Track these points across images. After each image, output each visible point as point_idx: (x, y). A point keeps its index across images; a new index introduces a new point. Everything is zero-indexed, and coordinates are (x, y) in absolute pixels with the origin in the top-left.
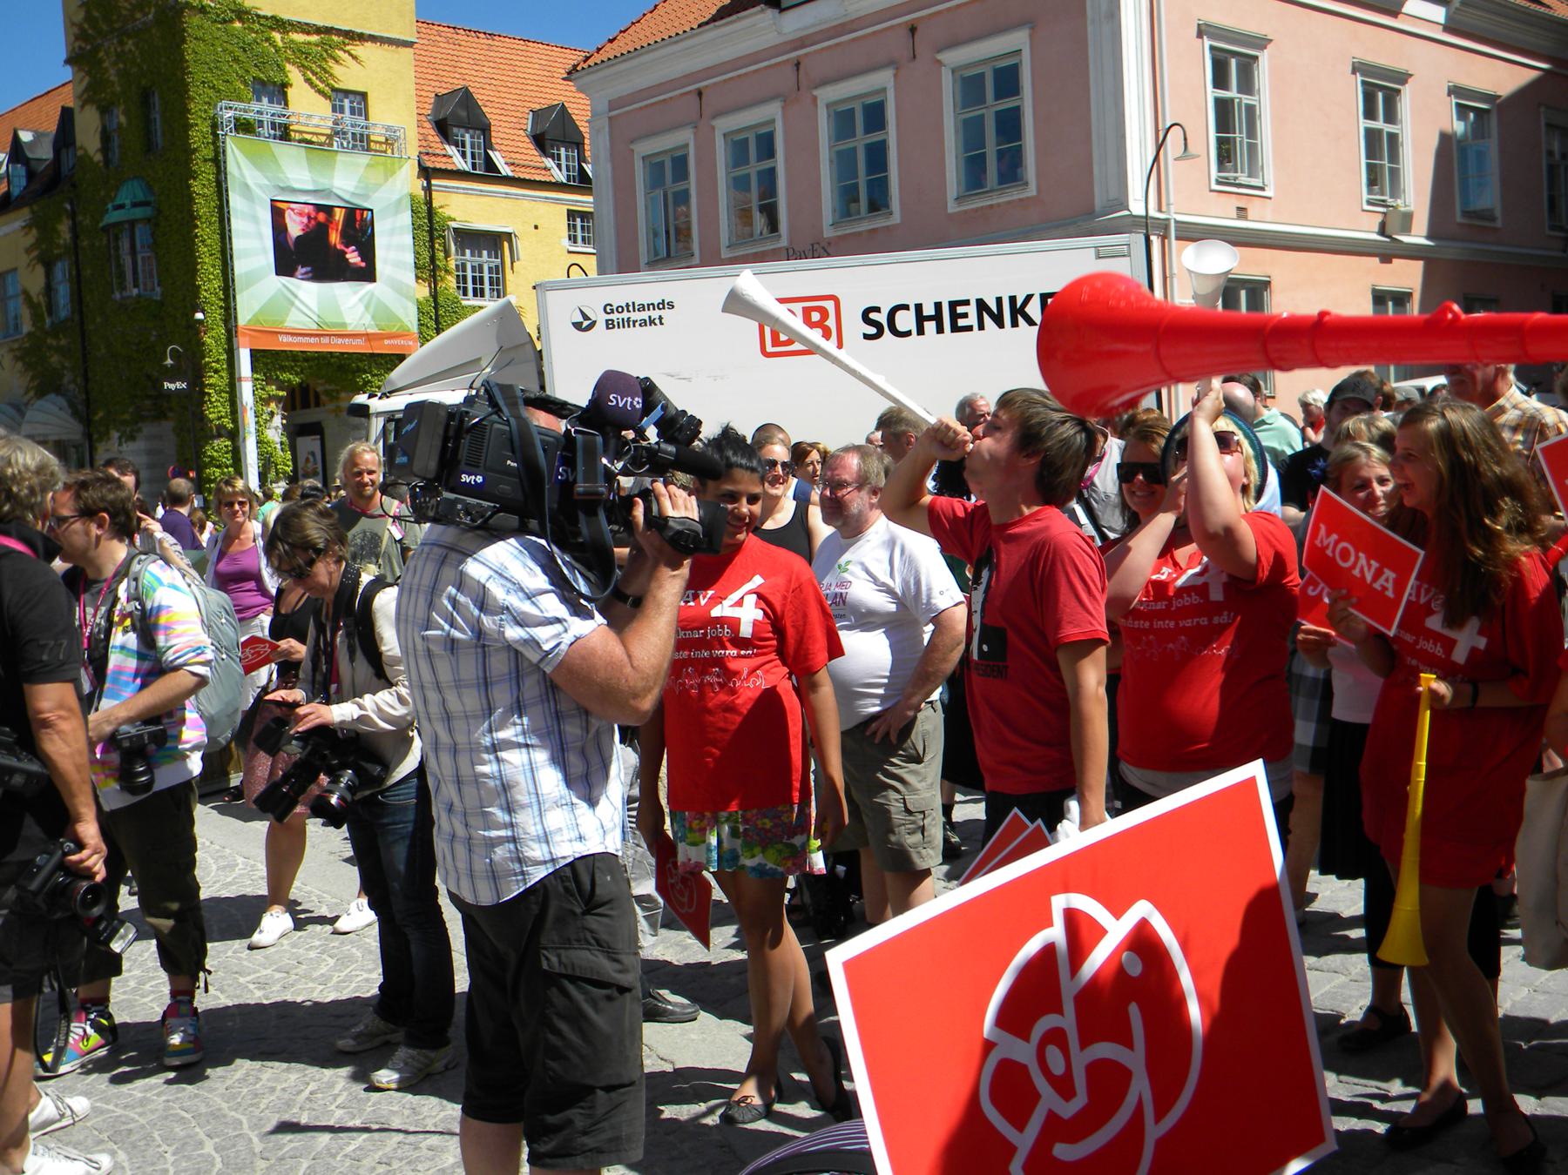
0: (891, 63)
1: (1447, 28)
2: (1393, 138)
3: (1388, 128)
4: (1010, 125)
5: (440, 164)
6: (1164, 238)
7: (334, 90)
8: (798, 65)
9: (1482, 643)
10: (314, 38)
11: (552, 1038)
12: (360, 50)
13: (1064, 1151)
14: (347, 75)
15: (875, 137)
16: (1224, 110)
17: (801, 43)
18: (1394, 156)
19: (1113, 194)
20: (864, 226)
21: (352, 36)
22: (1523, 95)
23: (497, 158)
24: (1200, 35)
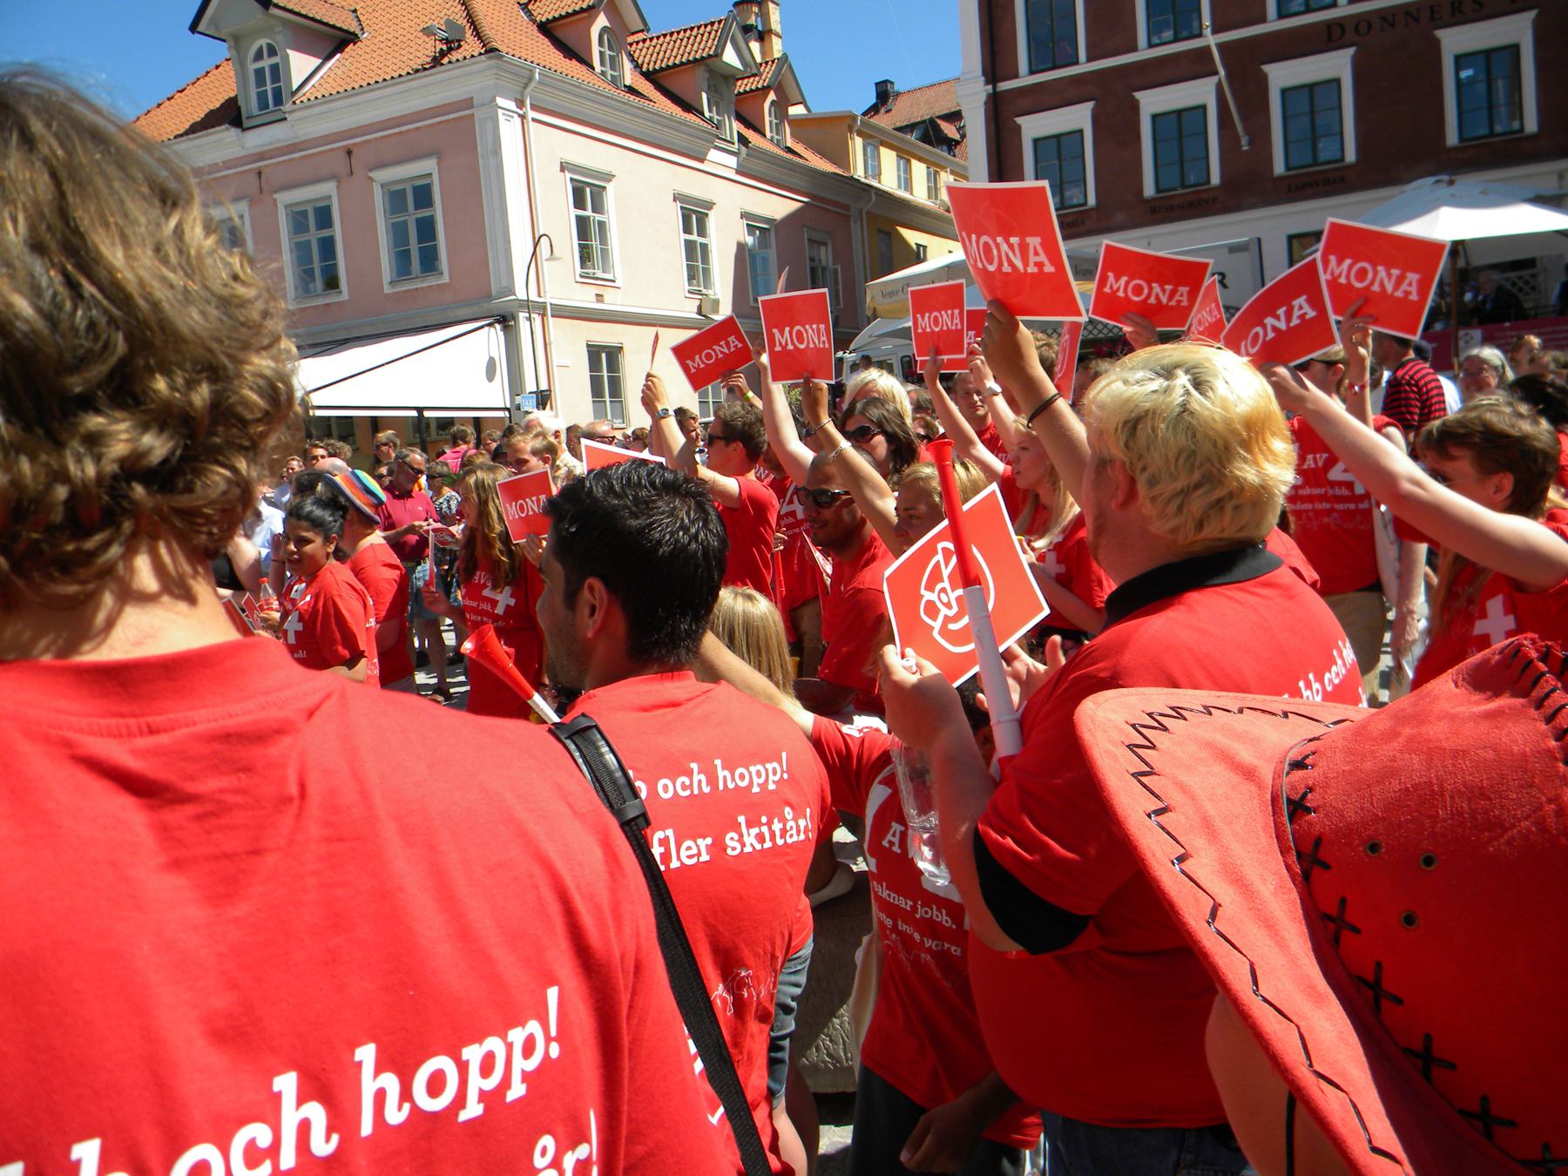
0: (333, 177)
1: (738, 172)
2: (704, 247)
3: (700, 240)
4: (427, 229)
6: (543, 316)
8: (260, 173)
9: (512, 602)
13: (952, 627)
15: (325, 233)
16: (582, 224)
17: (261, 156)
18: (706, 259)
19: (504, 283)
20: (321, 301)
22: (792, 218)
24: (562, 169)
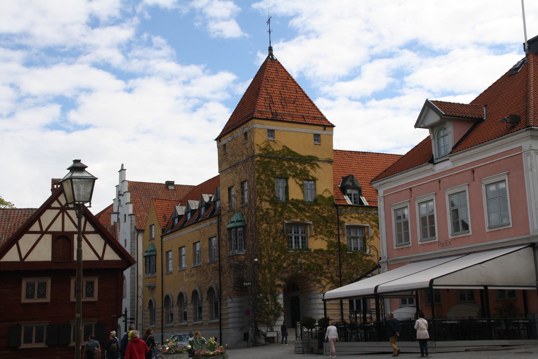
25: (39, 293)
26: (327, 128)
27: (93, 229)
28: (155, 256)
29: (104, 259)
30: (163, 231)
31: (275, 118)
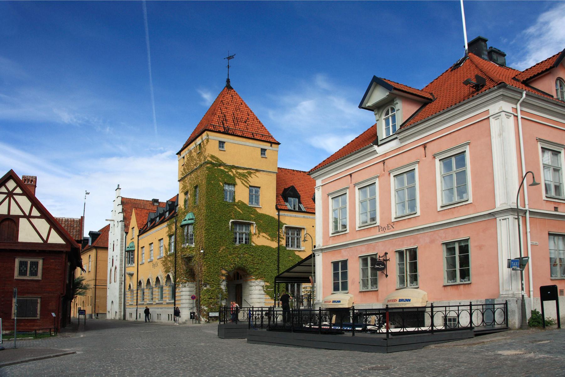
5: (283, 208)
7: (250, 186)
10: (245, 171)
11: (502, 357)
12: (257, 174)
14: (254, 180)
21: (257, 171)
23: (301, 206)
25: (31, 271)
26: (273, 145)
27: (38, 214)
28: (134, 251)
29: (49, 242)
30: (140, 231)
31: (226, 132)
